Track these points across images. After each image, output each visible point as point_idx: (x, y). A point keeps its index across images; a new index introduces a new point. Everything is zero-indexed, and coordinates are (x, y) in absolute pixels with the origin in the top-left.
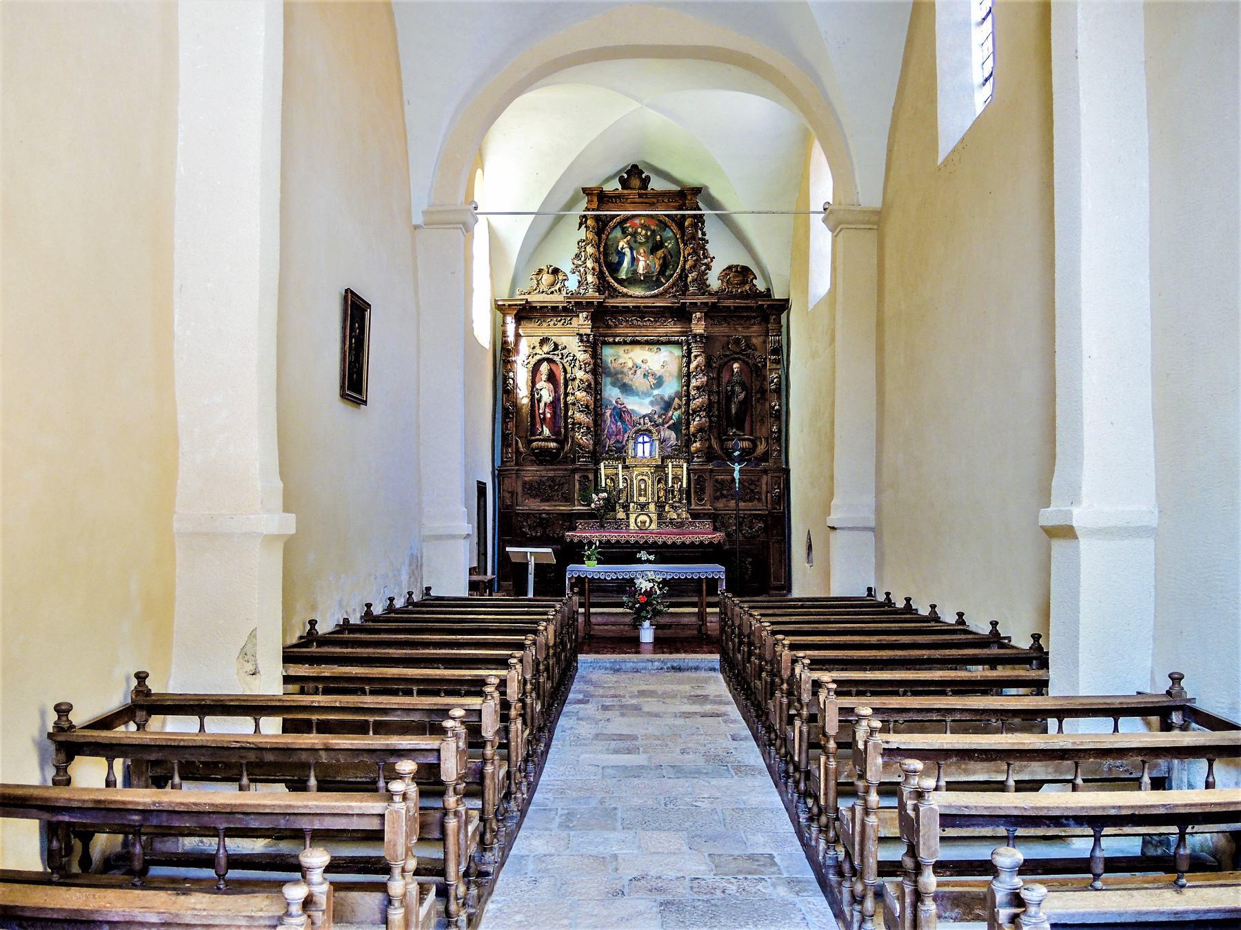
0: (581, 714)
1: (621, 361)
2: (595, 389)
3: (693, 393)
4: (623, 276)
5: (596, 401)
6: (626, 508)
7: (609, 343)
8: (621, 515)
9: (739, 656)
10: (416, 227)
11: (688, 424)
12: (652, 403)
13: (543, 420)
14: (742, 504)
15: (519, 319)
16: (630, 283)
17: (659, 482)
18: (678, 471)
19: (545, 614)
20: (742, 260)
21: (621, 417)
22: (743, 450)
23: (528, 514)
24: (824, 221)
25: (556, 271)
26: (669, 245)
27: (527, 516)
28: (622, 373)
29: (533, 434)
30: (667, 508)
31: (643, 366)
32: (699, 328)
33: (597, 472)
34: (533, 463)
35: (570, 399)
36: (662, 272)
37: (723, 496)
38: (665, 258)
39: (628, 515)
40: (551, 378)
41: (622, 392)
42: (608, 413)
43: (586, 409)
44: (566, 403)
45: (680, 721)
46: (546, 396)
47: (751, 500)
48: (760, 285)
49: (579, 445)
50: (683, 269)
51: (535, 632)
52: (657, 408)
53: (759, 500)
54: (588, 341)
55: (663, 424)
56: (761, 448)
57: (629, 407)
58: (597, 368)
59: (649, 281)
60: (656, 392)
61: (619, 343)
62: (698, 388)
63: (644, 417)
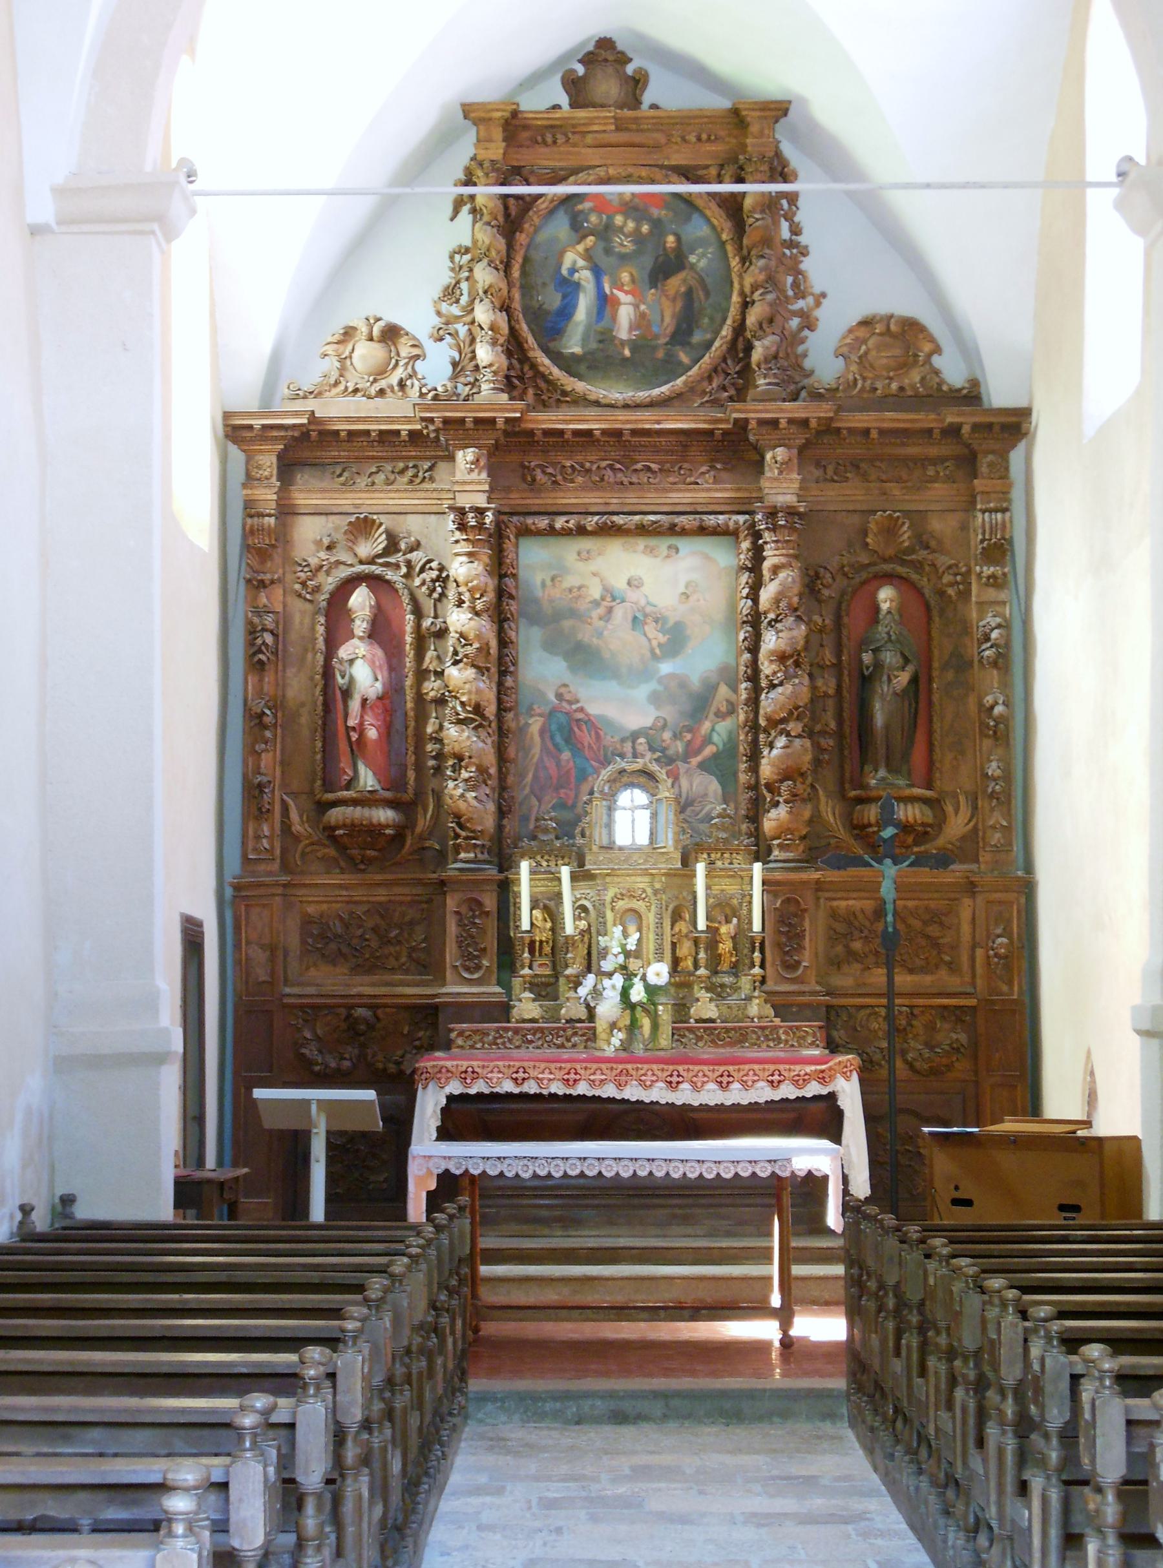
0: (486, 1517)
1: (570, 581)
2: (500, 662)
3: (767, 668)
4: (573, 346)
5: (501, 690)
7: (539, 533)
9: (898, 1366)
10: (36, 231)
11: (754, 757)
13: (358, 747)
14: (903, 980)
17: (676, 917)
19: (336, 1313)
20: (899, 300)
22: (906, 828)
23: (314, 1007)
24: (1120, 205)
25: (391, 334)
27: (312, 1011)
28: (573, 613)
29: (328, 786)
32: (781, 485)
33: (506, 889)
34: (330, 865)
35: (432, 687)
36: (681, 334)
38: (689, 295)
40: (381, 630)
41: (573, 668)
42: (535, 725)
43: (475, 716)
44: (420, 698)
45: (749, 1533)
48: (952, 370)
49: (458, 816)
50: (740, 328)
51: (332, 1342)
52: (669, 713)
53: (953, 967)
54: (481, 526)
55: (686, 758)
57: (593, 710)
58: (503, 603)
59: (645, 360)
60: (666, 668)
61: (566, 533)
62: (782, 658)
63: (634, 736)
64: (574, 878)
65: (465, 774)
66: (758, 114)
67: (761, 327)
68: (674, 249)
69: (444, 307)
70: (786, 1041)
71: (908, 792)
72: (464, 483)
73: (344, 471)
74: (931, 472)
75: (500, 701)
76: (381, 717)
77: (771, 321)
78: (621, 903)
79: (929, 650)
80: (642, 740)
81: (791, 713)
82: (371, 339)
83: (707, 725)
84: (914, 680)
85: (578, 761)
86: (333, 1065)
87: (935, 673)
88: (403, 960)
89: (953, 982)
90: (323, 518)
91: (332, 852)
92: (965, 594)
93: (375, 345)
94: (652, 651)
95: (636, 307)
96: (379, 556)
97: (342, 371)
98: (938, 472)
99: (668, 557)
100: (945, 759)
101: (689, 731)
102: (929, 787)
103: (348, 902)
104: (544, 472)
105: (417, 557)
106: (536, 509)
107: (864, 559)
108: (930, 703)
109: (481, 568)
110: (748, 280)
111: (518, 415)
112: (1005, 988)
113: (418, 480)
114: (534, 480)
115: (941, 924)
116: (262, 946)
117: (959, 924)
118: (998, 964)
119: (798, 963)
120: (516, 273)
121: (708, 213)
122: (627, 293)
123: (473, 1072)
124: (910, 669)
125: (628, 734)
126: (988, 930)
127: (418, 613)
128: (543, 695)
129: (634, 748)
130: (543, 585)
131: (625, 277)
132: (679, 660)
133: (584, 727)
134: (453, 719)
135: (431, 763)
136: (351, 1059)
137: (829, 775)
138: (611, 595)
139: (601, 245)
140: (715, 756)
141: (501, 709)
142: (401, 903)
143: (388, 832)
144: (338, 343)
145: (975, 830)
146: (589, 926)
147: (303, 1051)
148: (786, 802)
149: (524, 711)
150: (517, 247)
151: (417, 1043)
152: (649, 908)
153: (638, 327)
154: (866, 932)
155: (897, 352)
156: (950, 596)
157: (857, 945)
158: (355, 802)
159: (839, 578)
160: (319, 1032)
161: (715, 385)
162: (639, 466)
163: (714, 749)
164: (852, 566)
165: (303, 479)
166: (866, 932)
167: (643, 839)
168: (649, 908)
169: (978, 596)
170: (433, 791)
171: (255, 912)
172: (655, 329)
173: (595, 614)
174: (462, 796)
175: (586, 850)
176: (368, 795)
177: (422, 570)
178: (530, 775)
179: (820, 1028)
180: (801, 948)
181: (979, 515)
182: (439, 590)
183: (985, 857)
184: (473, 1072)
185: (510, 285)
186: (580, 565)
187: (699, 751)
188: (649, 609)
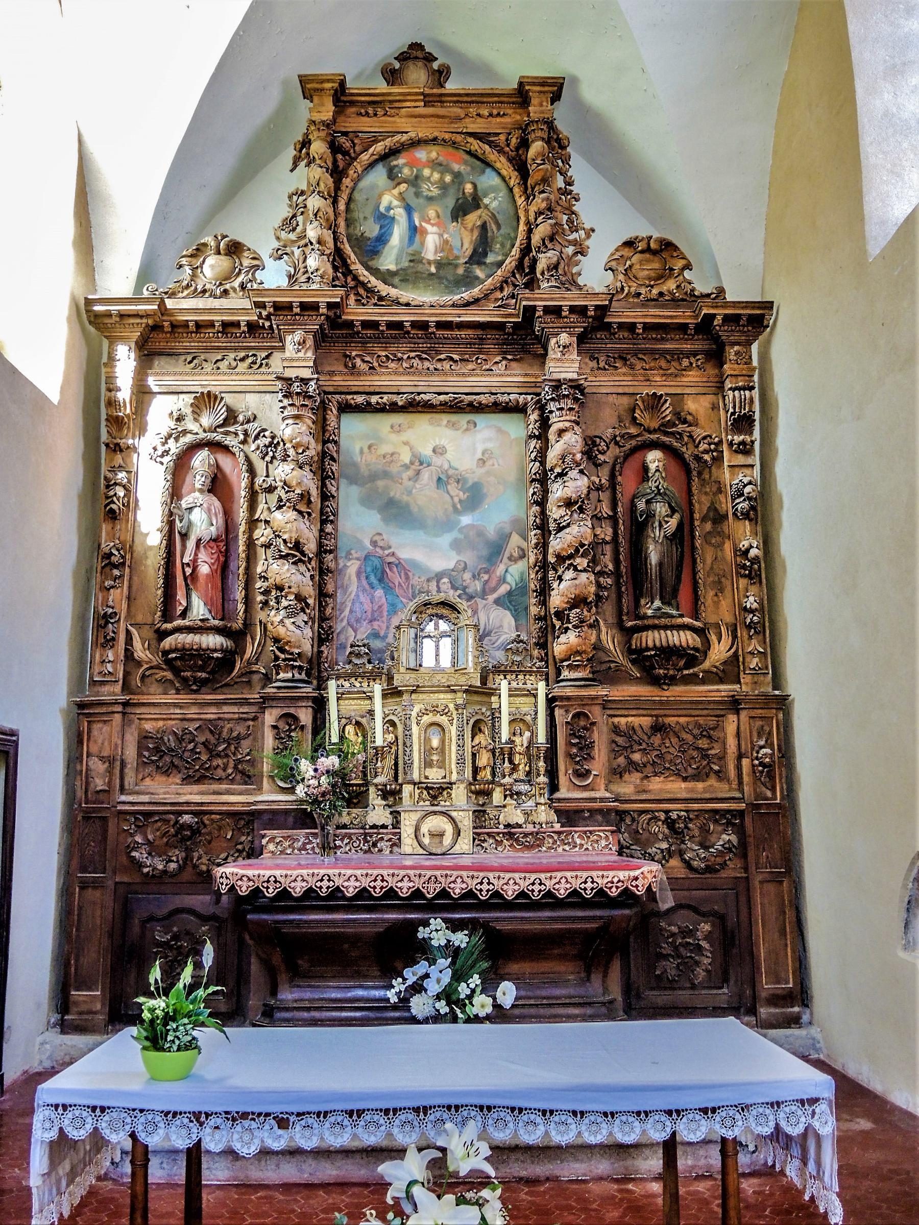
1: (385, 449)
2: (322, 508)
3: (555, 512)
6: (391, 794)
8: (378, 814)
11: (544, 592)
12: (456, 545)
15: (148, 353)
16: (404, 280)
17: (476, 729)
18: (522, 706)
21: (382, 578)
23: (148, 815)
25: (234, 249)
26: (494, 201)
28: (386, 475)
30: (497, 796)
31: (437, 461)
35: (262, 534)
36: (478, 257)
37: (633, 766)
38: (484, 227)
39: (396, 814)
40: (217, 485)
41: (386, 520)
42: (352, 568)
43: (295, 552)
44: (251, 544)
46: (202, 520)
47: (698, 776)
50: (526, 249)
52: (469, 557)
53: (721, 775)
55: (484, 594)
56: (719, 651)
57: (404, 554)
59: (445, 273)
60: (466, 520)
62: (568, 503)
63: (439, 577)
64: (385, 696)
65: (285, 603)
66: (538, 88)
67: (544, 243)
68: (471, 194)
69: (283, 235)
70: (581, 845)
71: (680, 621)
72: (292, 360)
73: (194, 358)
74: (685, 362)
75: (320, 545)
76: (215, 556)
77: (552, 239)
78: (425, 718)
79: (690, 504)
80: (445, 580)
81: (577, 550)
82: (219, 253)
83: (501, 568)
84: (680, 525)
85: (390, 597)
86: (160, 867)
87: (697, 523)
88: (230, 771)
89: (722, 789)
90: (175, 397)
91: (169, 675)
92: (718, 460)
93: (222, 257)
94: (454, 506)
95: (441, 235)
96: (218, 426)
97: (194, 277)
98: (691, 364)
99: (467, 430)
100: (708, 596)
101: (486, 572)
102: (697, 619)
103: (182, 720)
104: (363, 361)
105: (253, 428)
106: (354, 389)
107: (633, 431)
108: (693, 548)
109: (304, 428)
110: (533, 209)
111: (338, 300)
112: (769, 794)
113: (256, 366)
114: (354, 366)
115: (710, 737)
116: (102, 758)
117: (725, 738)
118: (762, 772)
119: (588, 772)
120: (342, 206)
121: (498, 165)
122: (433, 225)
123: (276, 882)
124: (677, 516)
125: (433, 575)
126: (752, 742)
127: (252, 471)
128: (360, 542)
129: (438, 586)
130: (362, 452)
131: (432, 213)
132: (477, 514)
133: (395, 569)
134: (277, 555)
135: (260, 598)
136: (178, 862)
137: (609, 608)
138: (420, 462)
139: (412, 190)
140: (510, 593)
141: (322, 550)
142: (229, 720)
143: (215, 655)
144: (192, 256)
145: (736, 655)
146: (396, 738)
147: (134, 854)
148: (575, 627)
149: (343, 555)
150: (343, 188)
151: (240, 847)
152: (451, 722)
153: (442, 251)
154: (644, 746)
155: (656, 265)
156: (706, 461)
157: (636, 757)
158: (189, 630)
159: (612, 445)
160: (150, 837)
161: (505, 293)
162: (442, 356)
163: (508, 588)
164: (622, 437)
165: (160, 363)
166: (644, 746)
167: (446, 661)
168: (451, 722)
169: (730, 461)
170: (260, 622)
171: (96, 727)
172: (456, 252)
173: (406, 475)
174: (282, 621)
175: (394, 671)
176: (199, 623)
177: (257, 437)
178: (348, 609)
179: (612, 832)
180: (590, 757)
181: (730, 393)
182: (271, 454)
183: (745, 679)
184: (276, 882)
185: (336, 215)
186: (393, 437)
187: (494, 590)
188: (451, 472)
